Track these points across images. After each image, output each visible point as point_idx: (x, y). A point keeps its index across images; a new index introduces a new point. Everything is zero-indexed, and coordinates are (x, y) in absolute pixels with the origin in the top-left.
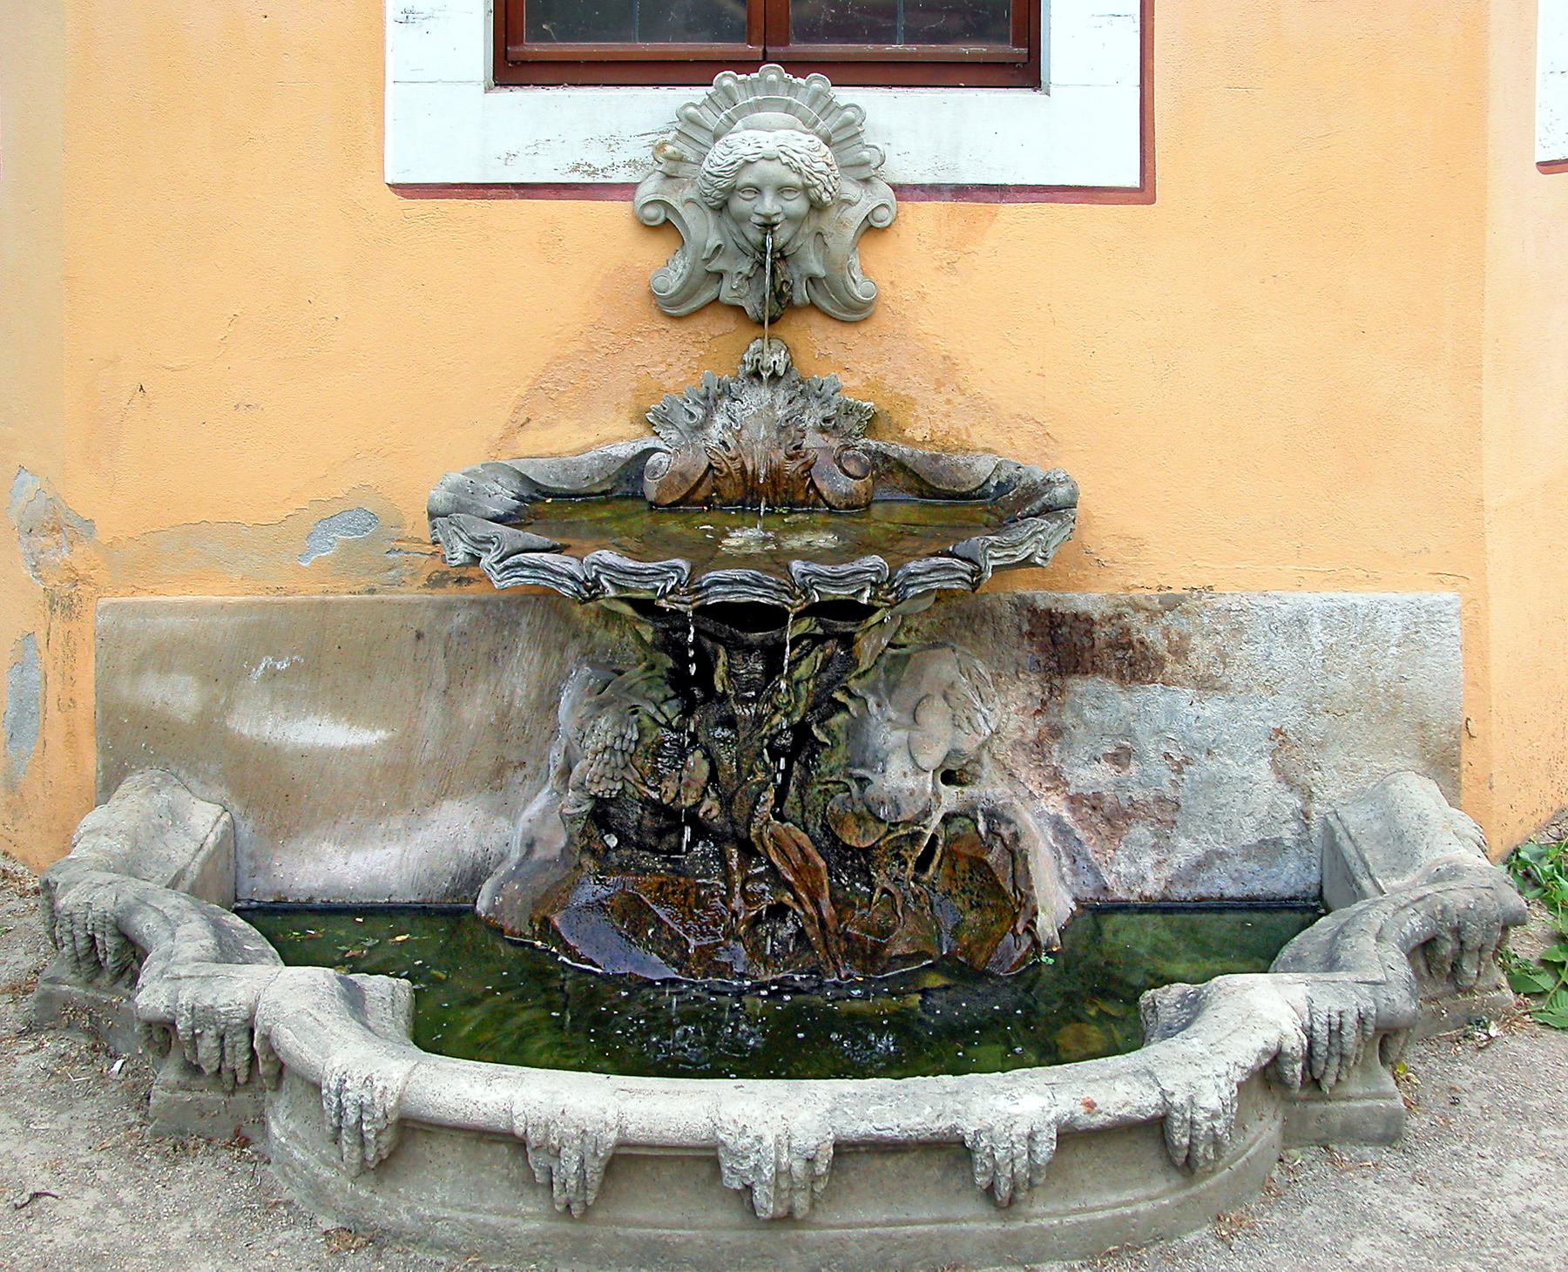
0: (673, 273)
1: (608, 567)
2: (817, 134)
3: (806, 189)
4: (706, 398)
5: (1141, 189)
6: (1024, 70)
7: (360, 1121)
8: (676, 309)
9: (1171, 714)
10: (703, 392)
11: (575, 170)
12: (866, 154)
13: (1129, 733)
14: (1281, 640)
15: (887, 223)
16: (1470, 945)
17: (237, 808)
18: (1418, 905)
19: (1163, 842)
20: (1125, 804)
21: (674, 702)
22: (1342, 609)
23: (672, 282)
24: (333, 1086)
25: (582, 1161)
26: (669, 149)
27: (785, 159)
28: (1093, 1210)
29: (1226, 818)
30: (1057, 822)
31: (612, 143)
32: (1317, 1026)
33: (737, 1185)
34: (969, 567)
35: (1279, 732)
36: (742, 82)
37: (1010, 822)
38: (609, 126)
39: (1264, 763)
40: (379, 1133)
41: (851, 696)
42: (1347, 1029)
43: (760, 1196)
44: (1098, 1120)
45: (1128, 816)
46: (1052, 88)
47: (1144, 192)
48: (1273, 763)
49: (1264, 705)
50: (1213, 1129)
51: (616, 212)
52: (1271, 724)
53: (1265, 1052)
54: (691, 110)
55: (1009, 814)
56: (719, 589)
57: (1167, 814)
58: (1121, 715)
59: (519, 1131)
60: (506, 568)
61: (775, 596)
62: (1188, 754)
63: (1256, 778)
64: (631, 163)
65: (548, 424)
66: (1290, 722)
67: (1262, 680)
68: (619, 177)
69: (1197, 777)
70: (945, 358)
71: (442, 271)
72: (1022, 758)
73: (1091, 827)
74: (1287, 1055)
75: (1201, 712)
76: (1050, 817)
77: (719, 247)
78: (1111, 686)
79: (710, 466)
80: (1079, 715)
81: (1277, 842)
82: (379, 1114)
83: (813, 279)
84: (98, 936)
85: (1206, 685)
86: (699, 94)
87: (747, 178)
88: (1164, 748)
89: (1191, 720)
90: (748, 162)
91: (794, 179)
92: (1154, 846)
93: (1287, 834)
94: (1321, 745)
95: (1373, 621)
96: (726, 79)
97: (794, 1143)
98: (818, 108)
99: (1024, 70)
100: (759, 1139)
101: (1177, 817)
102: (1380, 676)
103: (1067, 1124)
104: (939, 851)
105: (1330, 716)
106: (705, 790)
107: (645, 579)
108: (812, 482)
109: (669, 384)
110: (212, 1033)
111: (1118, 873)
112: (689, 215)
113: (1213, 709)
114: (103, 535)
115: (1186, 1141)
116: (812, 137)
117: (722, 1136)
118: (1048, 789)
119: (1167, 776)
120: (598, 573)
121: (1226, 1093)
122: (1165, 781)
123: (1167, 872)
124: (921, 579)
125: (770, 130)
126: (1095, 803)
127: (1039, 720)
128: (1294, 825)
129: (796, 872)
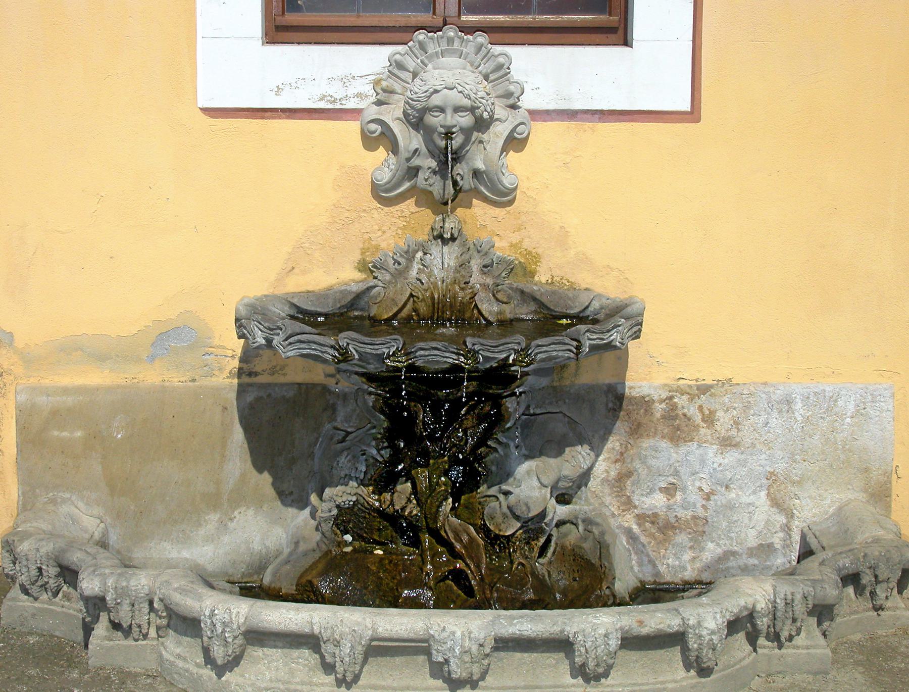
0: (379, 164)
1: (353, 340)
2: (480, 73)
3: (472, 110)
4: (407, 252)
5: (692, 112)
6: (618, 32)
7: (223, 631)
8: (383, 195)
9: (703, 462)
10: (406, 248)
11: (321, 99)
12: (512, 88)
13: (676, 473)
14: (775, 414)
15: (525, 135)
16: (881, 578)
17: (109, 520)
18: (849, 554)
19: (696, 545)
20: (673, 520)
21: (388, 450)
22: (815, 393)
23: (385, 176)
24: (207, 613)
25: (352, 647)
26: (384, 84)
27: (460, 89)
28: (643, 684)
29: (737, 530)
30: (629, 532)
31: (345, 80)
32: (778, 601)
33: (440, 659)
34: (575, 343)
35: (772, 473)
36: (432, 38)
37: (597, 524)
38: (347, 71)
39: (763, 494)
40: (235, 638)
41: (500, 443)
42: (796, 602)
43: (454, 665)
44: (645, 631)
45: (674, 528)
46: (634, 43)
47: (693, 115)
48: (768, 495)
49: (764, 456)
50: (712, 640)
51: (353, 128)
52: (768, 469)
53: (746, 608)
54: (398, 57)
55: (598, 520)
56: (422, 352)
57: (699, 528)
58: (671, 462)
59: (316, 631)
60: (290, 344)
61: (455, 357)
62: (714, 488)
63: (758, 503)
64: (359, 95)
65: (304, 272)
66: (780, 467)
67: (762, 439)
68: (351, 104)
69: (719, 503)
70: (561, 227)
71: (236, 190)
72: (607, 490)
73: (652, 536)
74: (759, 612)
75: (722, 461)
76: (625, 528)
77: (416, 150)
78: (664, 444)
79: (411, 295)
80: (644, 463)
81: (770, 546)
82: (235, 627)
83: (476, 173)
84: (44, 567)
85: (727, 443)
86: (400, 48)
87: (436, 100)
88: (698, 484)
89: (716, 465)
90: (436, 91)
91: (467, 102)
92: (691, 548)
93: (777, 540)
94: (799, 482)
95: (836, 401)
96: (421, 36)
97: (472, 636)
98: (480, 56)
99: (618, 32)
100: (453, 633)
101: (706, 529)
102: (840, 437)
103: (627, 632)
104: (553, 543)
105: (805, 463)
106: (409, 500)
107: (376, 347)
108: (476, 306)
109: (383, 245)
110: (128, 602)
111: (668, 565)
112: (398, 129)
113: (731, 457)
114: (19, 343)
115: (695, 646)
116: (476, 75)
117: (432, 632)
118: (624, 511)
119: (700, 502)
120: (348, 344)
121: (720, 621)
122: (699, 505)
123: (698, 565)
124: (545, 349)
125: (450, 73)
126: (653, 519)
127: (618, 466)
128: (781, 535)
129: (465, 547)
